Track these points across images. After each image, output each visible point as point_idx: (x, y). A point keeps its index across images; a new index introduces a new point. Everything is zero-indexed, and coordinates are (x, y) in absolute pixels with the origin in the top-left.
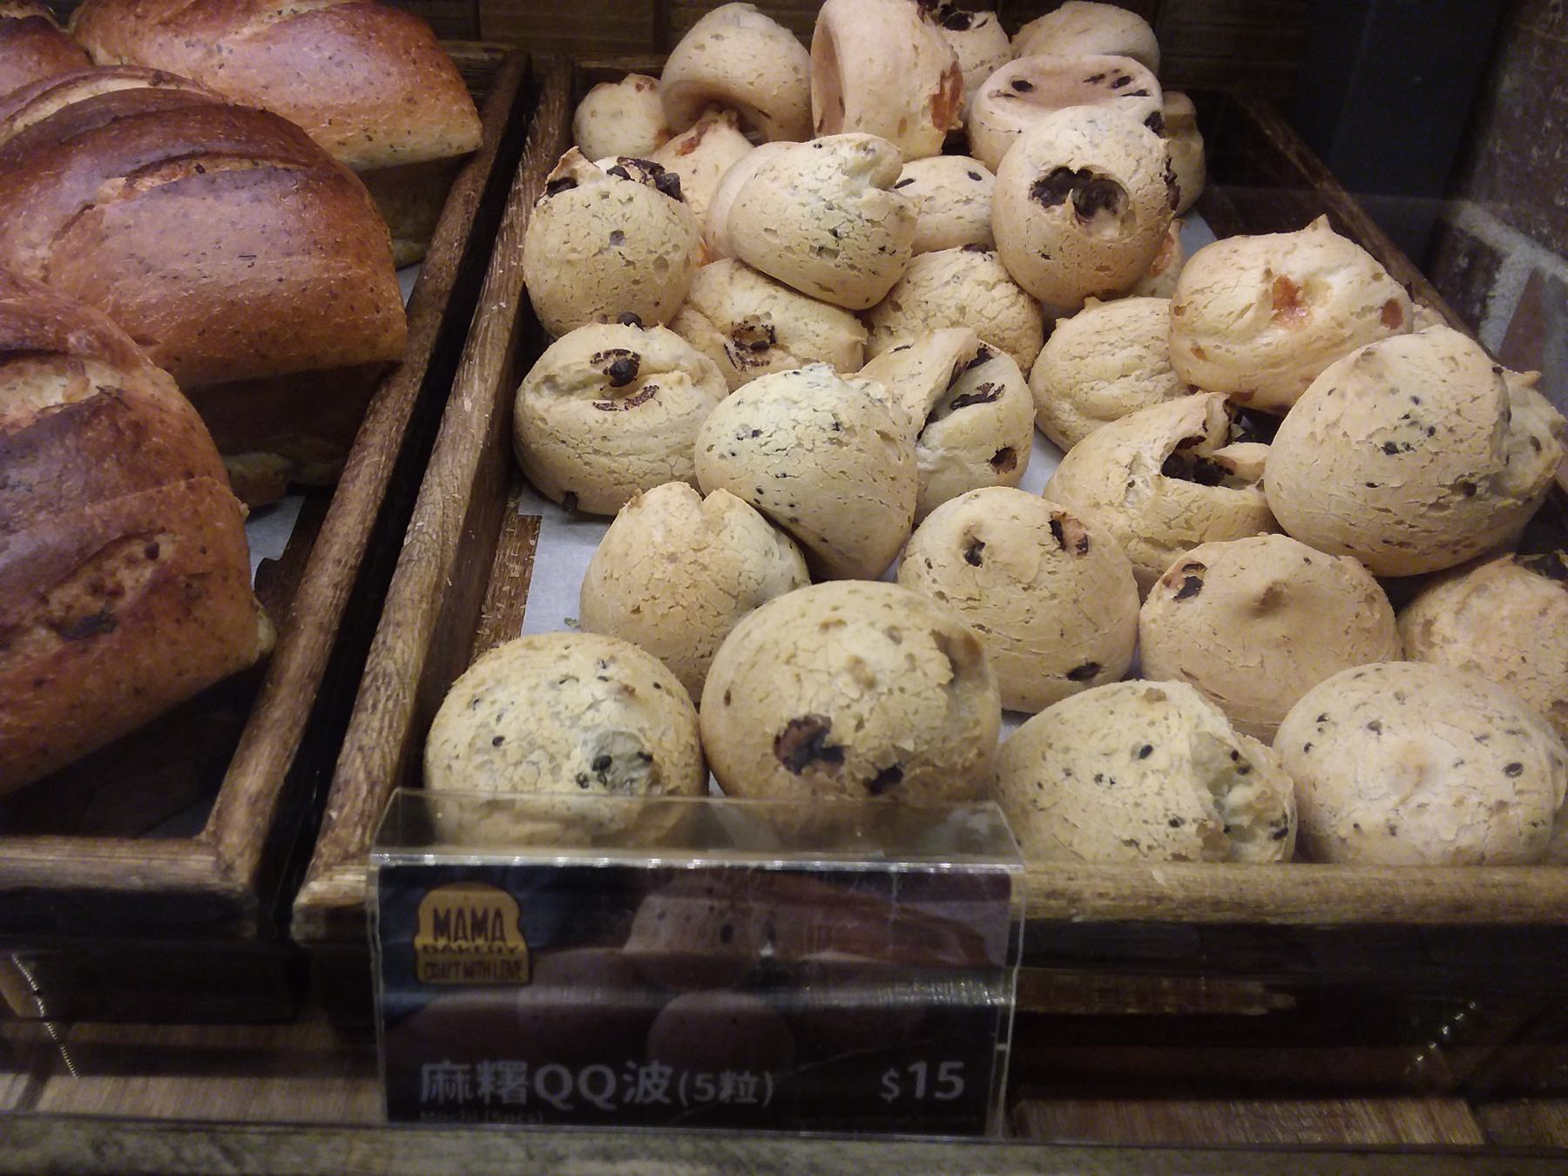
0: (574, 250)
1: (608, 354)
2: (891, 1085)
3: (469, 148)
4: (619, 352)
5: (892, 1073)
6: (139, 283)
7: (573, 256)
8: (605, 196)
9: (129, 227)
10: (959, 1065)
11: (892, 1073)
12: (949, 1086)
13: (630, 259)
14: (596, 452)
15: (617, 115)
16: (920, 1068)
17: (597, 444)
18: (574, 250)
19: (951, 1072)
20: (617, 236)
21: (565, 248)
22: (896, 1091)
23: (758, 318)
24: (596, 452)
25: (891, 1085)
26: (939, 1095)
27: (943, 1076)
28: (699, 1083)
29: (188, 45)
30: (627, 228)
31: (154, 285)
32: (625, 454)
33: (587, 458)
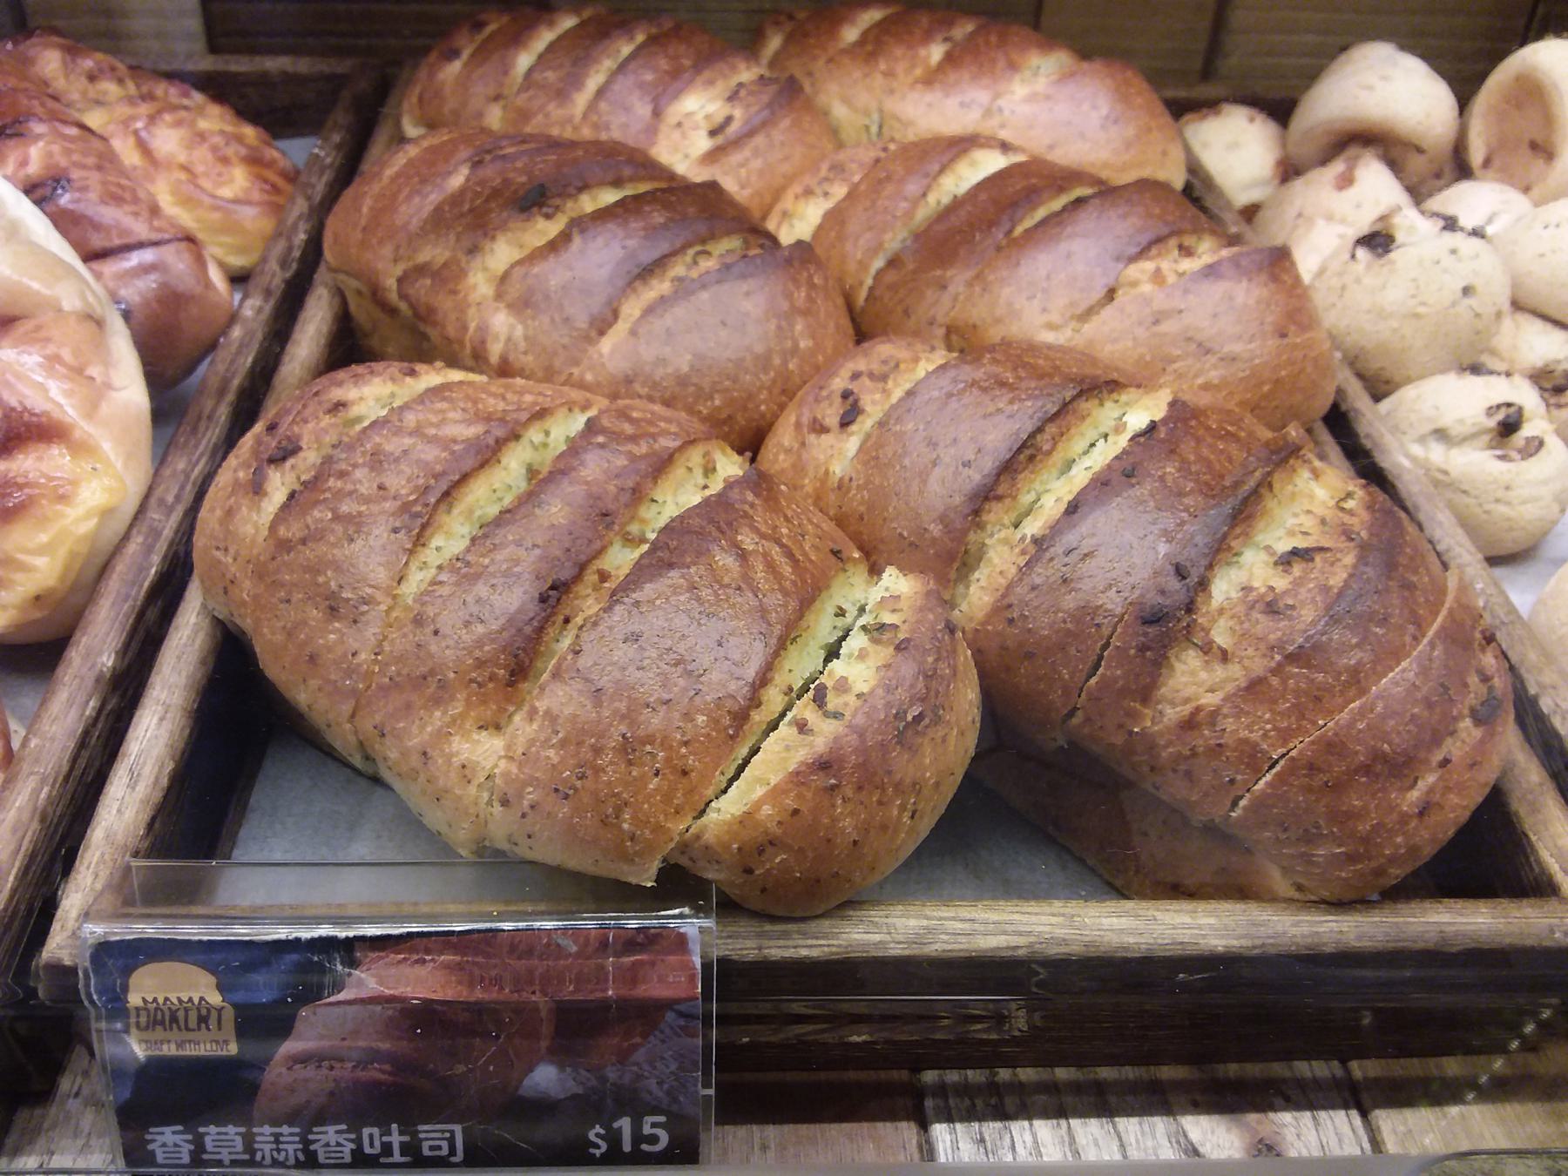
0: (1423, 304)
1: (1499, 407)
2: (600, 1142)
3: (156, 154)
4: (1509, 405)
5: (598, 1129)
6: (1198, 365)
7: (1421, 310)
8: (1454, 252)
9: (1181, 312)
10: (662, 1119)
11: (598, 1129)
12: (653, 1139)
13: (1479, 311)
14: (1497, 501)
15: (1234, 146)
16: (625, 1124)
17: (1500, 494)
18: (1423, 304)
19: (654, 1125)
20: (1467, 291)
21: (1414, 302)
22: (604, 1146)
23: (1559, 362)
24: (1497, 501)
25: (600, 1142)
26: (645, 1147)
27: (647, 1130)
28: (647, 1130)
29: (962, 104)
30: (1478, 283)
31: (1215, 367)
32: (1524, 502)
33: (1487, 507)
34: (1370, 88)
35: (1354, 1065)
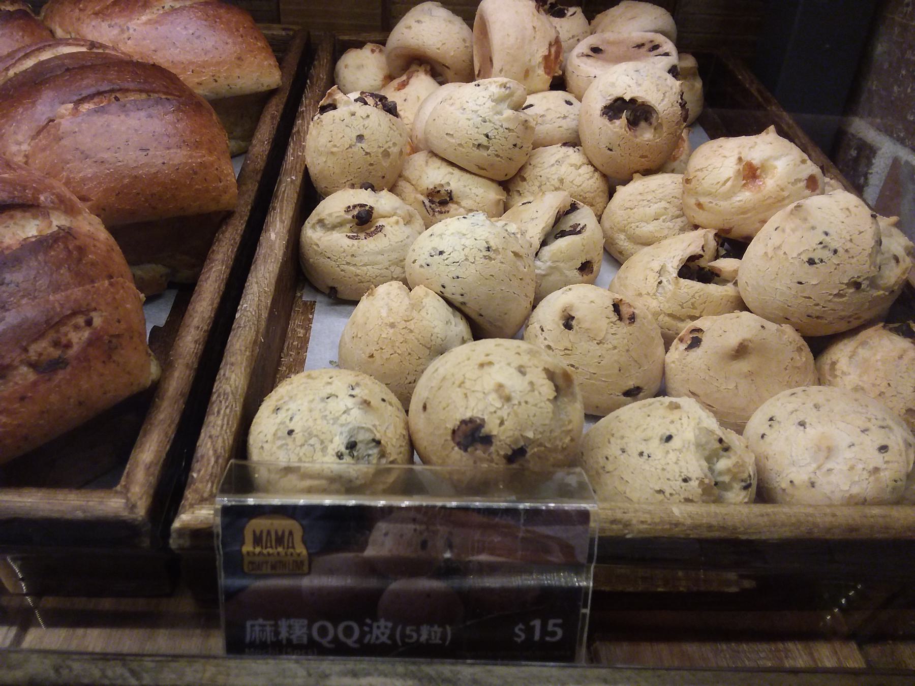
0: (335, 146)
1: (355, 207)
2: (520, 633)
4: (361, 206)
5: (521, 626)
6: (81, 165)
7: (335, 150)
8: (353, 114)
9: (75, 132)
10: (559, 621)
11: (521, 626)
12: (554, 634)
13: (368, 151)
14: (348, 264)
15: (360, 67)
16: (537, 623)
17: (349, 259)
18: (335, 146)
19: (555, 625)
20: (360, 138)
21: (329, 145)
22: (523, 636)
23: (442, 186)
24: (348, 264)
25: (520, 633)
26: (548, 639)
27: (550, 628)
28: (408, 632)
29: (110, 26)
30: (366, 133)
31: (90, 166)
32: (365, 265)
33: (342, 267)
34: (410, 27)
35: (283, 624)
